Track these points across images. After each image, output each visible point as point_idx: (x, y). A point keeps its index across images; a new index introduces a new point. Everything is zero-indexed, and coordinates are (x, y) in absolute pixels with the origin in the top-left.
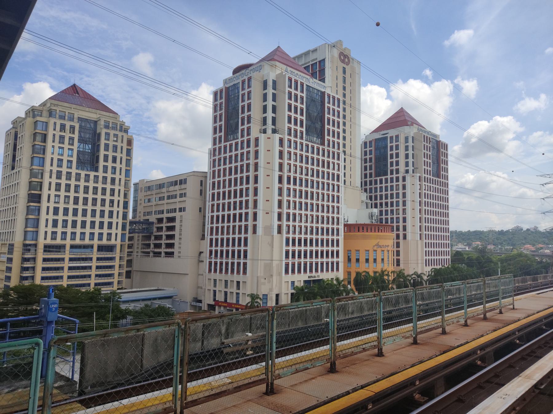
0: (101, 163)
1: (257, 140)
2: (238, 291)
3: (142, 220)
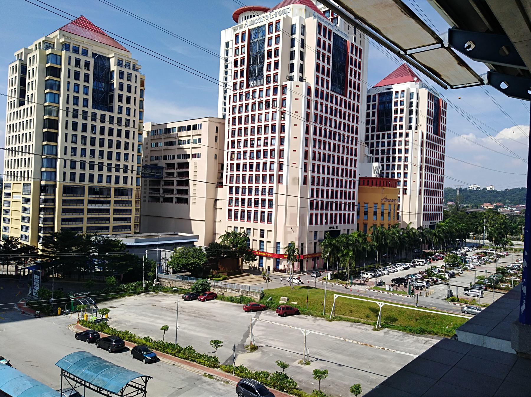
0: (116, 103)
1: (284, 87)
2: (262, 239)
3: (149, 164)
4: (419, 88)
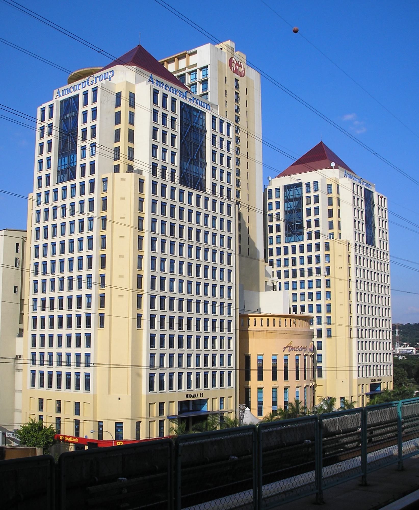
1: (105, 181)
4: (340, 177)
